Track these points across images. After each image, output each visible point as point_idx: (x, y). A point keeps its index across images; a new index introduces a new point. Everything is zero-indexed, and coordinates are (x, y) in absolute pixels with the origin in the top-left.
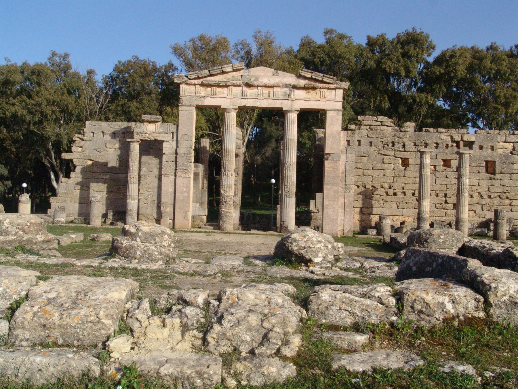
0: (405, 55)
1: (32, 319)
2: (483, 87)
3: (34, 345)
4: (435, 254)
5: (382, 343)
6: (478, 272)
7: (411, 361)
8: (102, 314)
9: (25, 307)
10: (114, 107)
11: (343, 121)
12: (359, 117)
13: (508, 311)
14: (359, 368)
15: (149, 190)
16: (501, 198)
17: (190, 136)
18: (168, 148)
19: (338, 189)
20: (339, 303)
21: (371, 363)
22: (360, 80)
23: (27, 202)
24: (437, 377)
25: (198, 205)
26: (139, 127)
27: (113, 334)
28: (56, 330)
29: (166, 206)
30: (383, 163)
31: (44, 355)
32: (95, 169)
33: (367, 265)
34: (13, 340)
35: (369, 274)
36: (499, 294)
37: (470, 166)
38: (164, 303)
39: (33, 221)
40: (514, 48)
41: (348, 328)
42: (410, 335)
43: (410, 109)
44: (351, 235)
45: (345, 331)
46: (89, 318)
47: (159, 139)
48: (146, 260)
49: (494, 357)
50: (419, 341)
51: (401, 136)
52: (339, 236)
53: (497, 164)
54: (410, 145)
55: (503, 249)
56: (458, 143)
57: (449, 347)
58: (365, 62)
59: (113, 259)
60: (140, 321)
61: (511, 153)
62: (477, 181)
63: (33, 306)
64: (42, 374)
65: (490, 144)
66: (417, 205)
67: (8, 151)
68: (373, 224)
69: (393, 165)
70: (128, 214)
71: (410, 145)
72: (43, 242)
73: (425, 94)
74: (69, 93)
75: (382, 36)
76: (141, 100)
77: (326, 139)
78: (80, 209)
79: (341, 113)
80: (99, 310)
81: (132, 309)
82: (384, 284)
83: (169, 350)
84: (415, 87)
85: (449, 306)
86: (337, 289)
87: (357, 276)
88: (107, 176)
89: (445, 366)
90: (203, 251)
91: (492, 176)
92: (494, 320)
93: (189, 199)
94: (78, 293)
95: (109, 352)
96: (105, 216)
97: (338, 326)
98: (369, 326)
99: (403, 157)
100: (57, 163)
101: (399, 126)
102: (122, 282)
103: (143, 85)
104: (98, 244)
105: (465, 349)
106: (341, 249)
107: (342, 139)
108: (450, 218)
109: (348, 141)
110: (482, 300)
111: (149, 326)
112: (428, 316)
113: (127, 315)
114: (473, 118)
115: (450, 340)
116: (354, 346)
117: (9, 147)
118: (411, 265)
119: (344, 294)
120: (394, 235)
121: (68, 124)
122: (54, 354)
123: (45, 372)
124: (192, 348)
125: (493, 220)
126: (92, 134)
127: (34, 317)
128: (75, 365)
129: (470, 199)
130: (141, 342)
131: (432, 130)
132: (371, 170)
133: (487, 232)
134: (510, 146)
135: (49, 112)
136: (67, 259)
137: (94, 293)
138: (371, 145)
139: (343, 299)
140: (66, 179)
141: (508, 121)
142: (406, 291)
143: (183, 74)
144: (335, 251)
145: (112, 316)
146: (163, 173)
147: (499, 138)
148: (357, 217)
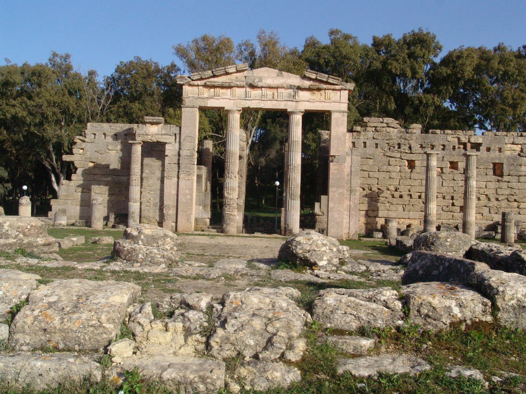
0: (411, 55)
1: (33, 324)
2: (490, 88)
3: (34, 350)
4: (442, 257)
5: (388, 348)
6: (485, 275)
7: (418, 365)
8: (103, 318)
9: (26, 311)
10: (115, 109)
11: (349, 122)
12: (365, 119)
13: (516, 315)
14: (365, 373)
15: (152, 193)
16: (508, 201)
17: (193, 138)
18: (171, 150)
19: (344, 191)
20: (345, 307)
21: (377, 367)
22: (366, 81)
23: (27, 205)
24: (444, 382)
25: (201, 207)
26: (141, 129)
27: (114, 339)
28: (57, 334)
29: (169, 208)
30: (389, 165)
31: (44, 360)
32: (97, 171)
33: (373, 268)
34: (13, 345)
35: (374, 278)
36: (506, 298)
37: (477, 168)
38: (167, 307)
39: (34, 224)
40: (522, 49)
41: (353, 332)
42: (416, 339)
43: (416, 110)
44: (356, 238)
45: (350, 335)
46: (90, 322)
47: (162, 141)
48: (148, 263)
49: (502, 362)
50: (426, 346)
51: (407, 138)
52: (345, 239)
53: (504, 166)
54: (416, 147)
55: (511, 252)
56: (465, 145)
57: (456, 352)
58: (371, 62)
59: (114, 263)
60: (142, 326)
61: (519, 155)
62: (485, 183)
63: (33, 310)
64: (43, 379)
65: (497, 146)
66: (423, 207)
67: (8, 153)
68: (379, 227)
69: (399, 167)
70: (130, 216)
71: (416, 147)
72: (44, 245)
73: (432, 95)
74: (71, 94)
75: (388, 37)
76: (143, 101)
77: (332, 140)
78: (82, 211)
79: (346, 114)
80: (100, 314)
81: (134, 313)
82: (390, 288)
83: (172, 355)
84: (421, 88)
85: (456, 310)
86: (342, 293)
87: (363, 280)
88: (109, 179)
89: (452, 371)
90: (206, 254)
91: (500, 178)
92: (502, 324)
93: (192, 202)
94: (79, 297)
95: (111, 357)
96: (106, 219)
97: (343, 330)
98: (374, 330)
99: (410, 159)
100: (58, 165)
101: (405, 128)
102: (124, 286)
103: (145, 87)
104: (100, 247)
105: (472, 354)
106: (346, 253)
107: (347, 141)
108: (457, 221)
109: (354, 143)
110: (490, 304)
111: (151, 330)
112: (435, 320)
113: (129, 319)
114: (480, 120)
115: (457, 344)
116: (360, 351)
117: (9, 149)
118: (418, 268)
119: (349, 298)
120: (400, 238)
121: (69, 125)
122: (55, 358)
123: (46, 377)
124: (195, 352)
125: (500, 223)
126: (93, 136)
127: (34, 321)
128: (76, 370)
129: (477, 201)
130: (143, 346)
131: (438, 131)
132: (377, 172)
133: (494, 235)
134: (518, 148)
135: (50, 114)
136: (68, 262)
137: (96, 297)
138: (377, 147)
139: (348, 303)
140: (67, 181)
141: (516, 123)
142: (412, 295)
143: (186, 75)
144: (340, 255)
145: (114, 320)
146: (165, 175)
147: (507, 140)
148: (363, 220)
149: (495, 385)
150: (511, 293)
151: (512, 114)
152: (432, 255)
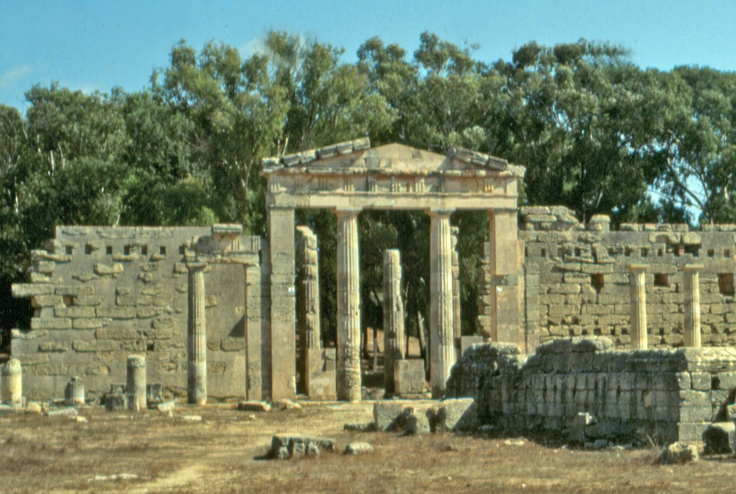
19: (517, 330)
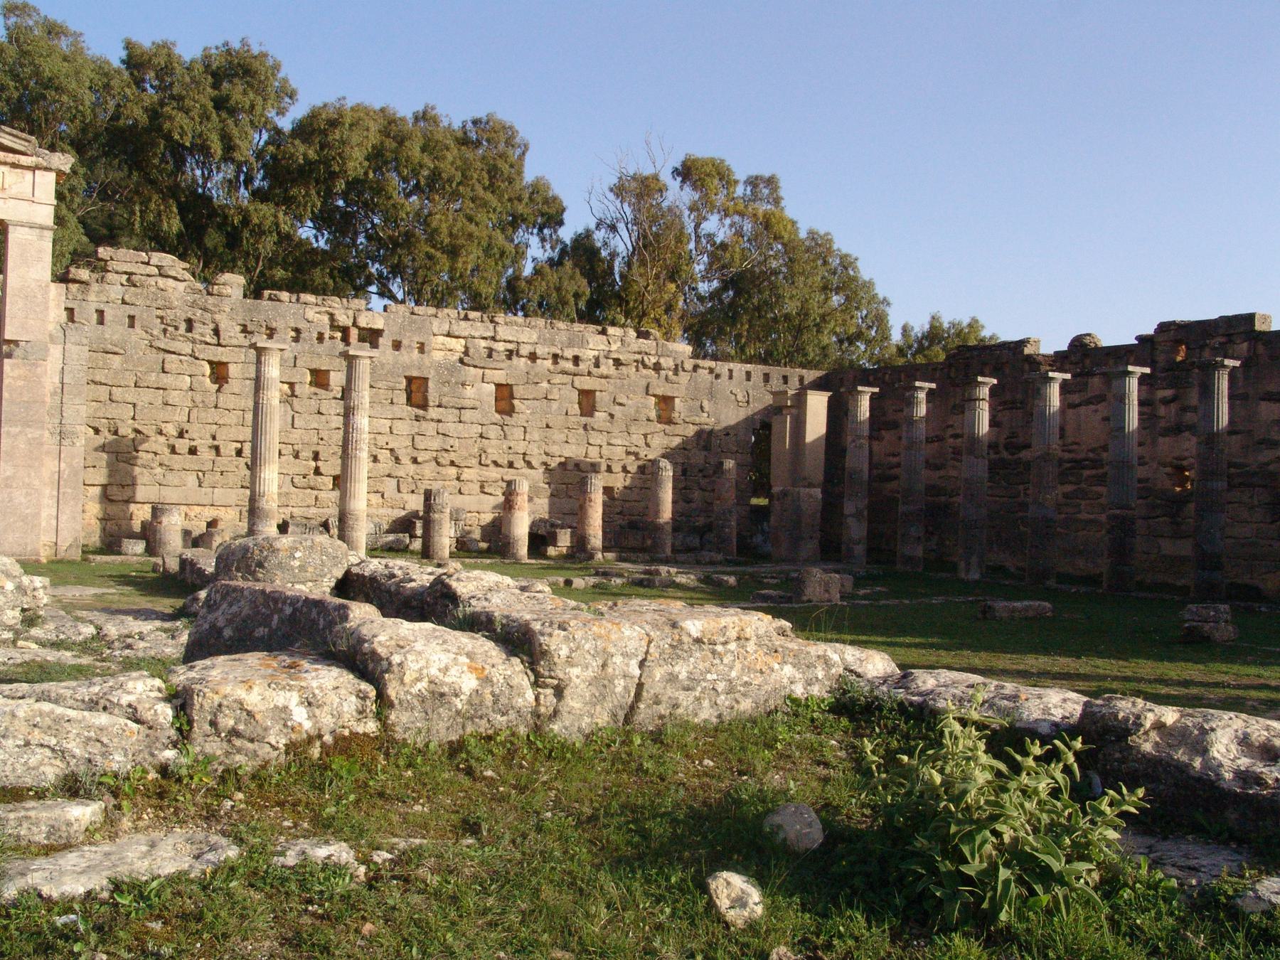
0: (220, 104)
2: (403, 205)
4: (276, 595)
5: (140, 818)
6: (365, 631)
7: (210, 850)
11: (57, 257)
12: (101, 250)
13: (427, 713)
14: (77, 887)
16: (438, 463)
19: (42, 436)
20: (24, 729)
21: (109, 868)
22: (106, 154)
24: (269, 881)
30: (164, 372)
33: (112, 630)
35: (117, 653)
36: (407, 679)
37: (371, 387)
40: (469, 126)
41: (48, 790)
42: (208, 790)
43: (233, 240)
44: (77, 555)
45: (40, 798)
49: (395, 818)
50: (230, 803)
51: (210, 307)
52: (44, 561)
53: (431, 384)
54: (231, 332)
55: (432, 578)
56: (345, 331)
57: (300, 809)
58: (118, 106)
61: (461, 361)
62: (388, 423)
65: (416, 339)
66: (248, 478)
68: (137, 526)
69: (188, 379)
71: (231, 332)
73: (272, 205)
75: (165, 48)
77: (8, 299)
79: (49, 235)
82: (146, 673)
84: (246, 188)
85: (300, 715)
86: (20, 694)
87: (86, 660)
89: (288, 853)
91: (421, 412)
92: (397, 736)
97: (22, 789)
98: (104, 779)
99: (216, 359)
101: (205, 280)
105: (334, 809)
106: (41, 593)
107: (52, 304)
108: (326, 510)
109: (70, 311)
110: (373, 693)
112: (252, 741)
114: (380, 274)
115: (301, 792)
116: (64, 835)
118: (220, 623)
119: (37, 706)
120: (189, 553)
125: (421, 514)
129: (371, 464)
131: (285, 295)
132: (133, 389)
133: (408, 541)
134: (458, 345)
138: (132, 326)
139: (34, 716)
141: (456, 289)
142: (198, 687)
144: (25, 599)
147: (436, 326)
148: (94, 509)
149: (379, 870)
150: (416, 668)
151: (446, 269)
152: (256, 591)
